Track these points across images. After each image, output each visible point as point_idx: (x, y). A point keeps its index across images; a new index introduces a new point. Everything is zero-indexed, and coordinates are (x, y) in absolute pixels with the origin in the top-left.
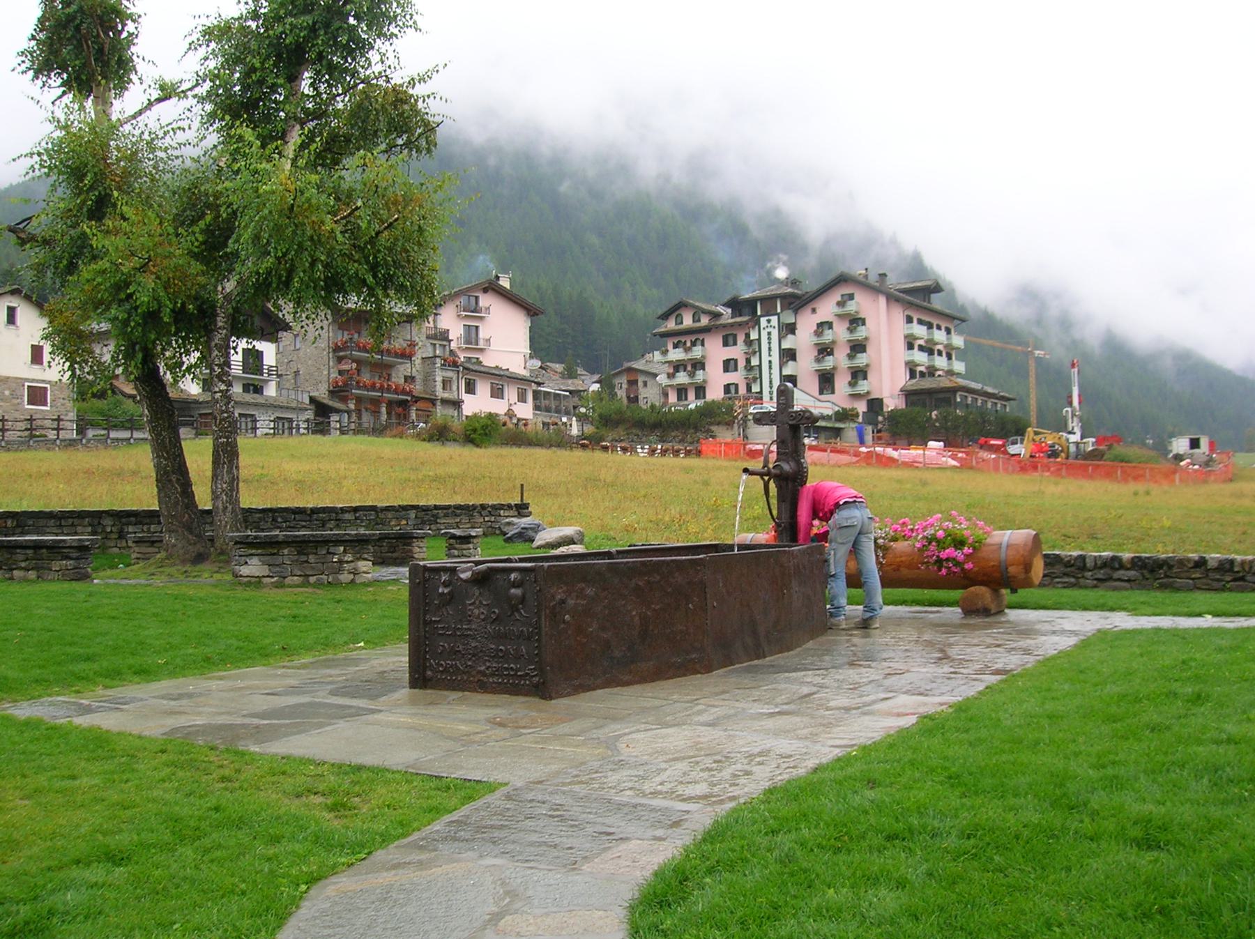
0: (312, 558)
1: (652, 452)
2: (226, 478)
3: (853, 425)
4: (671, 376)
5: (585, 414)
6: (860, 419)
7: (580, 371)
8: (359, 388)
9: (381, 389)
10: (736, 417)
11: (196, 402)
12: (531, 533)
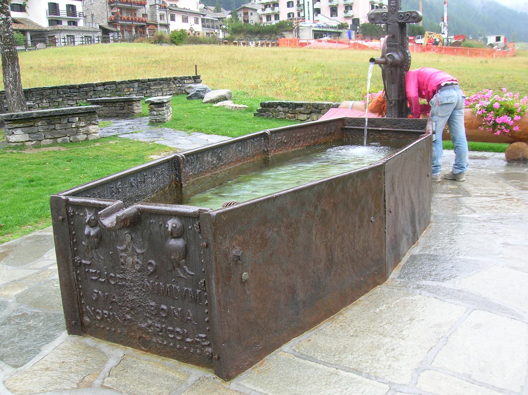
0: (58, 127)
1: (257, 45)
2: (11, 74)
3: (346, 31)
4: (263, 10)
5: (226, 29)
6: (349, 28)
7: (222, 9)
8: (122, 20)
9: (132, 21)
10: (294, 28)
11: (46, 31)
12: (201, 93)
